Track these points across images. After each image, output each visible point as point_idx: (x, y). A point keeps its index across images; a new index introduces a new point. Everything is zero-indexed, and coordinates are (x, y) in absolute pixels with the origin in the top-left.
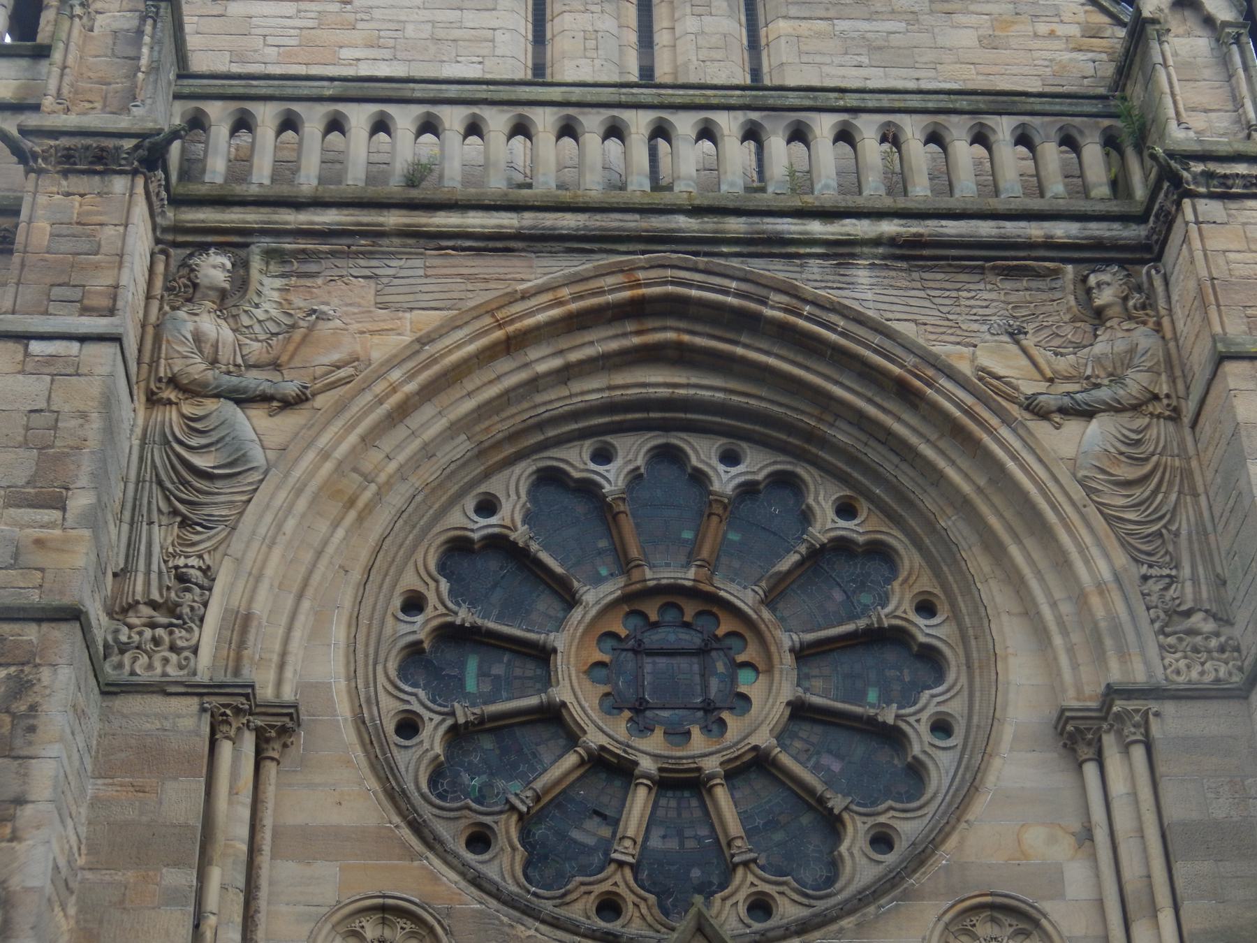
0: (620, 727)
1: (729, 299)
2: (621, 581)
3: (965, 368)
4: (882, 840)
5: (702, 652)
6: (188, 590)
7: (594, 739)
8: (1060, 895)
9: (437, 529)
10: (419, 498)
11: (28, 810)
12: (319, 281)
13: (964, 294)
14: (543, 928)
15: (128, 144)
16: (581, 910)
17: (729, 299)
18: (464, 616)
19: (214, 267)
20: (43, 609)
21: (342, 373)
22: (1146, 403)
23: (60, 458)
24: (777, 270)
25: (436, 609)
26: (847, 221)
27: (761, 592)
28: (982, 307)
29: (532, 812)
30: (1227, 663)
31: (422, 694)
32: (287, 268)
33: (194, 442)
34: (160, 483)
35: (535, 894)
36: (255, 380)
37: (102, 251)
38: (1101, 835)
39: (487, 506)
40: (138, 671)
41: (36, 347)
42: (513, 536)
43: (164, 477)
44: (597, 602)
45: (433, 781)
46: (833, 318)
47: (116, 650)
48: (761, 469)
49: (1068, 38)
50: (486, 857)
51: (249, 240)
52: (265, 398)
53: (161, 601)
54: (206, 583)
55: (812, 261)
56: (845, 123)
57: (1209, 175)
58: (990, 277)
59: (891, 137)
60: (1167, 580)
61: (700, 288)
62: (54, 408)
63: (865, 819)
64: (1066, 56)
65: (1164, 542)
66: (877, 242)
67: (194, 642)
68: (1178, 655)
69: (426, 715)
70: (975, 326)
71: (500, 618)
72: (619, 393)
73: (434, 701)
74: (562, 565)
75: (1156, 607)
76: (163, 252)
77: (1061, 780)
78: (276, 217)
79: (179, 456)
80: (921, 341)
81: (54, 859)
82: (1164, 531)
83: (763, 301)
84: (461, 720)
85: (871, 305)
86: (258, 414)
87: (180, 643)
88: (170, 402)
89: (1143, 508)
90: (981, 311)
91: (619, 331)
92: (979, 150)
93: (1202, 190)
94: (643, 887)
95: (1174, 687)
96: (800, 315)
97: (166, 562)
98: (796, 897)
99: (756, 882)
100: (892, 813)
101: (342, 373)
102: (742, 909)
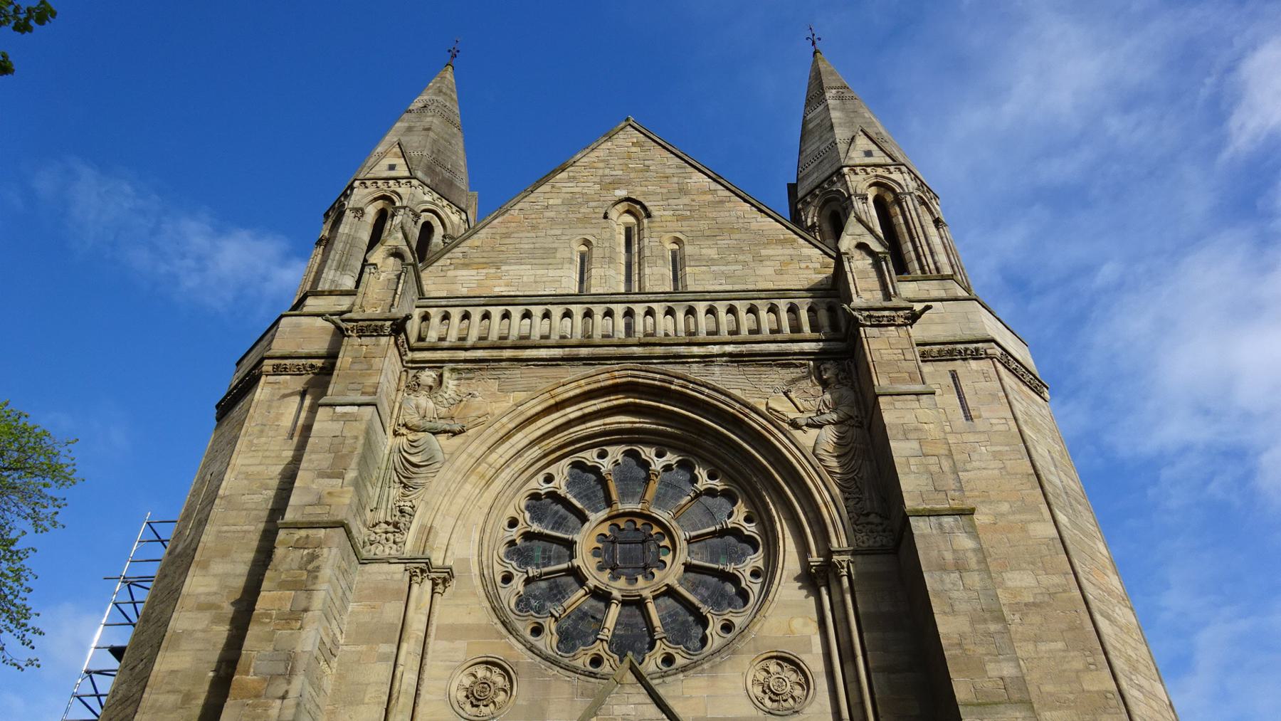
0: (605, 576)
1: (656, 383)
2: (608, 510)
3: (763, 408)
4: (727, 627)
5: (643, 542)
6: (404, 516)
7: (592, 583)
8: (810, 651)
11: (310, 613)
12: (474, 381)
13: (763, 376)
14: (561, 670)
15: (388, 323)
16: (582, 661)
17: (656, 383)
18: (536, 528)
19: (427, 376)
20: (327, 523)
21: (481, 420)
22: (847, 420)
23: (343, 457)
24: (678, 369)
25: (522, 525)
26: (709, 346)
27: (672, 514)
28: (771, 381)
29: (562, 616)
30: (886, 537)
31: (514, 564)
32: (460, 376)
33: (413, 451)
34: (395, 470)
35: (561, 656)
36: (441, 424)
37: (374, 368)
39: (549, 479)
40: (377, 553)
41: (338, 409)
42: (559, 492)
43: (397, 466)
44: (596, 520)
45: (517, 604)
46: (703, 389)
47: (369, 544)
48: (674, 459)
49: (815, 269)
50: (539, 638)
51: (444, 365)
52: (445, 432)
53: (391, 521)
54: (412, 513)
55: (693, 365)
56: (711, 306)
57: (870, 317)
58: (775, 368)
59: (732, 310)
60: (857, 500)
61: (643, 378)
62: (343, 435)
63: (718, 617)
64: (814, 276)
65: (856, 483)
66: (723, 355)
67: (404, 539)
68: (863, 534)
69: (515, 573)
70: (768, 390)
71: (552, 529)
72: (608, 426)
73: (520, 567)
74: (582, 504)
75: (852, 512)
76: (405, 371)
78: (456, 355)
79: (404, 457)
80: (743, 397)
81: (321, 638)
82: (855, 477)
83: (671, 383)
84: (531, 575)
85: (720, 382)
86: (442, 438)
87: (397, 540)
88: (403, 435)
89: (845, 467)
90: (771, 384)
92: (772, 316)
93: (869, 323)
94: (613, 652)
95: (860, 549)
96: (688, 388)
97: (395, 504)
98: (685, 655)
99: (665, 648)
100: (731, 614)
101: (481, 420)
102: (659, 661)
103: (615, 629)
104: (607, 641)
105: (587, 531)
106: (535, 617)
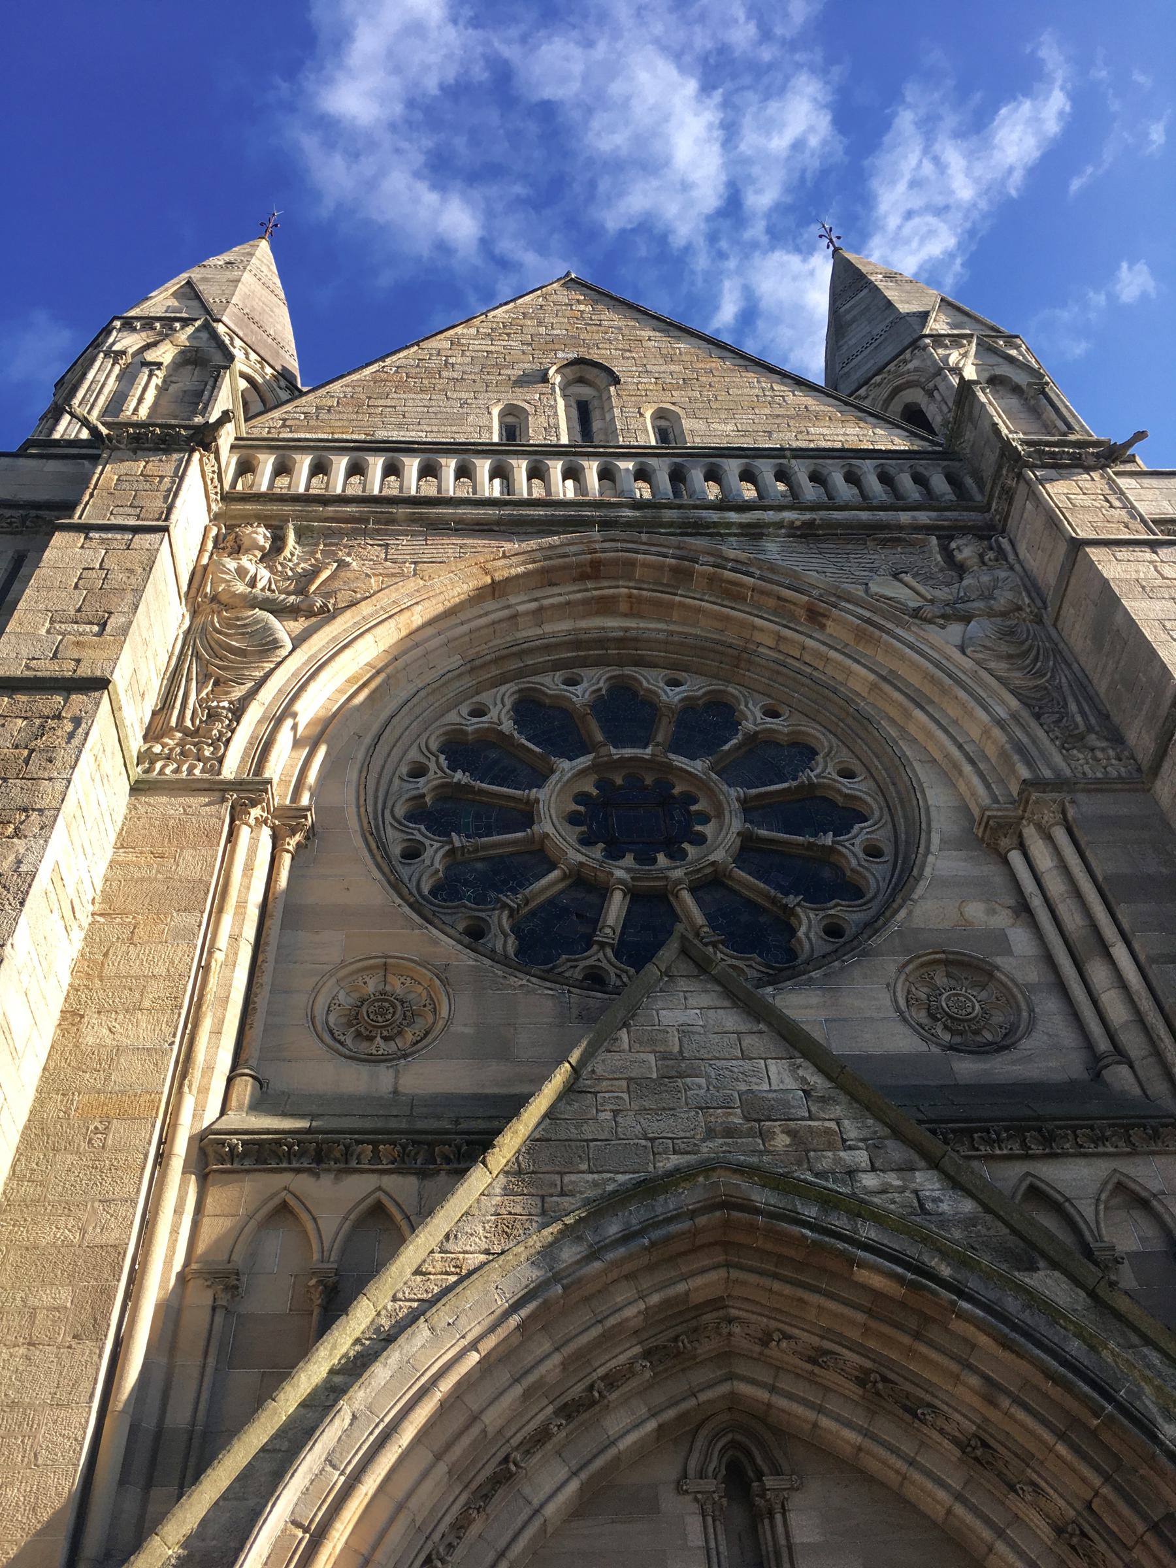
8: (1009, 952)
9: (437, 724)
10: (422, 694)
14: (534, 980)
25: (436, 773)
38: (1036, 902)
39: (479, 712)
48: (700, 688)
56: (747, 464)
77: (990, 870)
91: (583, 587)
103: (622, 933)
104: (611, 945)
105: (556, 784)
106: (470, 909)
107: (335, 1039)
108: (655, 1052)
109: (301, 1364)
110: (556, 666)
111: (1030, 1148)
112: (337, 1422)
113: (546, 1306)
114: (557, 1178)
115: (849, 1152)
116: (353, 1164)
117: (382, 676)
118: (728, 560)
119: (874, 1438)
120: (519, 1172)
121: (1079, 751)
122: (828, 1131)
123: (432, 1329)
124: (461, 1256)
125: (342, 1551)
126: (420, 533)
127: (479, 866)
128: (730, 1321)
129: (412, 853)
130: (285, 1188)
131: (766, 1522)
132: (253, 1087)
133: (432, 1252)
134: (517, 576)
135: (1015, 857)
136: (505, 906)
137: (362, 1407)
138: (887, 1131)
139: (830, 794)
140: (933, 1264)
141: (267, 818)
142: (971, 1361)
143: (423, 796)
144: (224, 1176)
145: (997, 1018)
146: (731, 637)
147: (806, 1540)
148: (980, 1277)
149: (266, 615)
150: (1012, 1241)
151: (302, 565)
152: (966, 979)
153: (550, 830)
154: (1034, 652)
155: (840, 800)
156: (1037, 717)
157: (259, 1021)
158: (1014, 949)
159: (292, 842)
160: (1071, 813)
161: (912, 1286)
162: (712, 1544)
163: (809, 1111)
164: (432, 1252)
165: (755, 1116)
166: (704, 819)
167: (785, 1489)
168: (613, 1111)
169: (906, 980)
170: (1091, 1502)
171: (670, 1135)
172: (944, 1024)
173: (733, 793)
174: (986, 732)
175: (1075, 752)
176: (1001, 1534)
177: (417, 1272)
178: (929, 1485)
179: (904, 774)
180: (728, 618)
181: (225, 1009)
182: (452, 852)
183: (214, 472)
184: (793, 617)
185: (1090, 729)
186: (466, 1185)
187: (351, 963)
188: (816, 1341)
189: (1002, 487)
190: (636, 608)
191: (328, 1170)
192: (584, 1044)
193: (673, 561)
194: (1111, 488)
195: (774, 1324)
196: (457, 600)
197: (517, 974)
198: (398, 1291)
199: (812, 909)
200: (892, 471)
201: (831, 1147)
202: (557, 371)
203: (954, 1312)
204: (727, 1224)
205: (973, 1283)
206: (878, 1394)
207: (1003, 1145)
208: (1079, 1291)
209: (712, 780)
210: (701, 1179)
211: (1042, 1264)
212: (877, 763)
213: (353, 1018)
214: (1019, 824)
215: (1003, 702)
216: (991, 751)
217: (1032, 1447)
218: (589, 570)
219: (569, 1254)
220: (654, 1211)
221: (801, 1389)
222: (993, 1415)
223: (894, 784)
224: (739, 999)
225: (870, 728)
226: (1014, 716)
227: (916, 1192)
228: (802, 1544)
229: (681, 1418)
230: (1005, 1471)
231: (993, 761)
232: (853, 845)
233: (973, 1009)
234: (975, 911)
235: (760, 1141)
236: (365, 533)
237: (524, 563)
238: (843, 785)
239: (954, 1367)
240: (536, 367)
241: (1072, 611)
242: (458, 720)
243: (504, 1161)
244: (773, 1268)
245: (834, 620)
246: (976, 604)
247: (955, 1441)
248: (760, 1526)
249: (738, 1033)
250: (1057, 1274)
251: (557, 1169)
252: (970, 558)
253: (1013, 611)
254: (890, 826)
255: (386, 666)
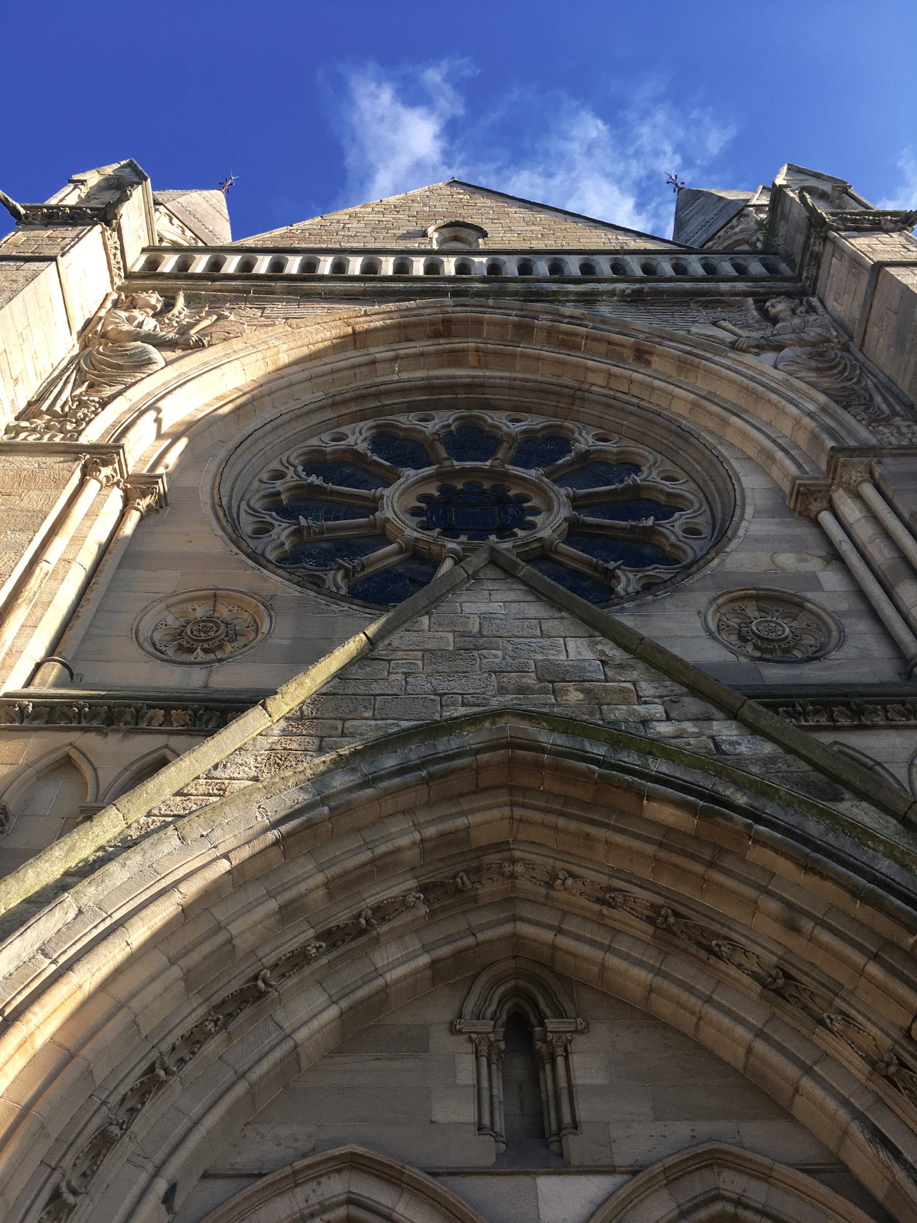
8: (820, 588)
38: (846, 548)
77: (804, 531)
107: (157, 649)
108: (454, 632)
109: (31, 861)
110: (411, 407)
111: (838, 721)
112: (58, 913)
113: (309, 826)
114: (339, 724)
115: (643, 706)
116: (144, 726)
117: (248, 396)
118: (564, 316)
119: (666, 976)
120: (302, 717)
121: (884, 426)
122: (623, 690)
123: (182, 839)
124: (227, 782)
125: (45, 1046)
126: (295, 301)
127: (325, 545)
128: (513, 861)
129: (263, 529)
130: (71, 744)
131: (548, 1067)
132: (61, 672)
133: (198, 778)
134: (376, 330)
135: (826, 518)
136: (341, 567)
137: (91, 904)
138: (685, 690)
139: (655, 496)
140: (727, 793)
141: (119, 481)
142: (770, 887)
143: (278, 494)
144: (12, 733)
145: (808, 640)
146: (566, 380)
147: (588, 1081)
148: (779, 805)
149: (150, 348)
150: (815, 776)
151: (187, 320)
152: (777, 611)
153: (390, 514)
154: (842, 366)
155: (662, 499)
156: (845, 408)
157: (79, 628)
158: (824, 586)
159: (144, 503)
160: (878, 471)
161: (704, 814)
162: (485, 1084)
163: (605, 675)
164: (198, 778)
165: (547, 677)
166: (536, 512)
167: (569, 1032)
168: (405, 673)
169: (717, 610)
170: (910, 1029)
171: (459, 691)
172: (754, 644)
173: (563, 491)
174: (797, 422)
175: (881, 428)
176: (808, 1070)
177: (179, 793)
178: (727, 1022)
179: (721, 468)
180: (563, 363)
181: (46, 610)
182: (298, 532)
183: (116, 248)
184: (622, 359)
185: (895, 414)
186: (241, 722)
187: (182, 593)
188: (604, 880)
189: (811, 255)
190: (483, 358)
191: (118, 731)
192: (382, 620)
193: (516, 318)
194: (908, 240)
195: (559, 864)
196: (321, 345)
197: (340, 603)
198: (154, 808)
199: (630, 571)
200: (715, 262)
201: (626, 701)
202: (435, 230)
203: (750, 837)
204: (511, 762)
205: (770, 809)
206: (669, 930)
207: (810, 718)
208: (889, 818)
209: (544, 483)
210: (487, 724)
211: (847, 795)
212: (698, 467)
213: (180, 633)
214: (828, 491)
215: (812, 400)
216: (802, 439)
217: (841, 975)
218: (441, 328)
219: (340, 781)
220: (435, 748)
221: (588, 931)
222: (795, 943)
223: (712, 480)
224: (543, 594)
225: (691, 439)
226: (824, 409)
227: (712, 738)
228: (584, 1085)
229: (457, 955)
230: (811, 1004)
231: (804, 449)
232: (673, 526)
233: (784, 632)
234: (788, 560)
235: (553, 697)
236: (246, 300)
237: (383, 319)
238: (666, 485)
239: (751, 893)
240: (418, 228)
241: (876, 329)
242: (319, 443)
243: (287, 709)
244: (559, 808)
245: (659, 355)
246: (788, 336)
247: (754, 975)
248: (541, 1074)
249: (539, 619)
250: (864, 804)
251: (340, 715)
252: (784, 310)
253: (823, 342)
254: (708, 513)
255: (252, 390)
